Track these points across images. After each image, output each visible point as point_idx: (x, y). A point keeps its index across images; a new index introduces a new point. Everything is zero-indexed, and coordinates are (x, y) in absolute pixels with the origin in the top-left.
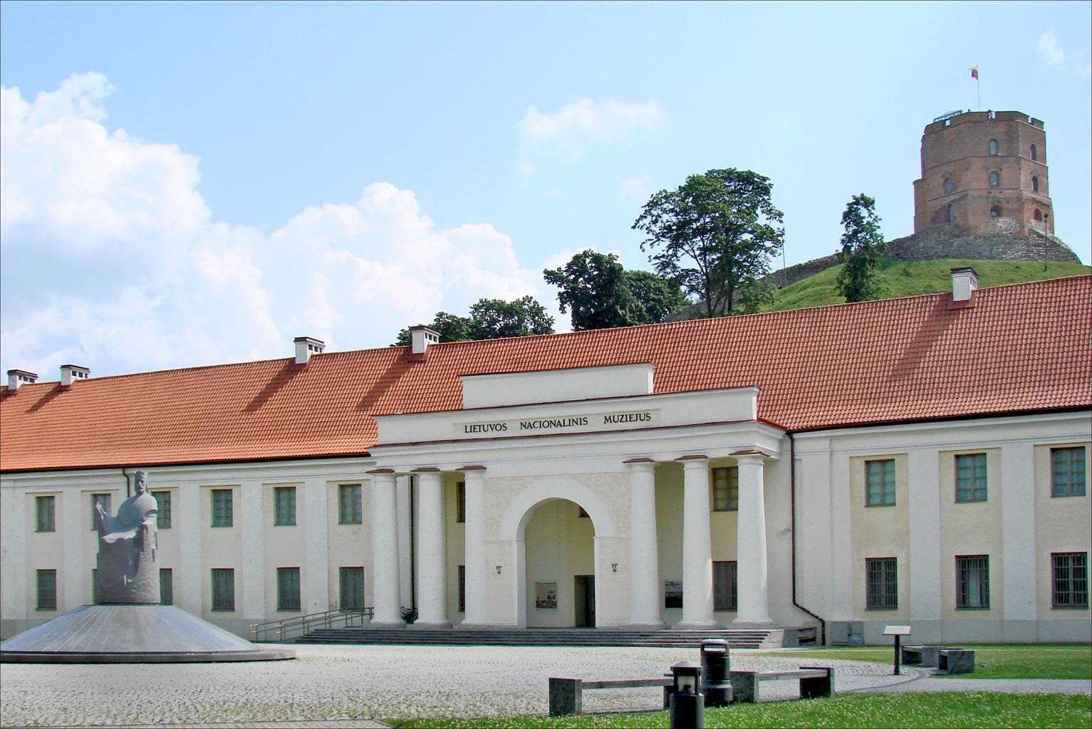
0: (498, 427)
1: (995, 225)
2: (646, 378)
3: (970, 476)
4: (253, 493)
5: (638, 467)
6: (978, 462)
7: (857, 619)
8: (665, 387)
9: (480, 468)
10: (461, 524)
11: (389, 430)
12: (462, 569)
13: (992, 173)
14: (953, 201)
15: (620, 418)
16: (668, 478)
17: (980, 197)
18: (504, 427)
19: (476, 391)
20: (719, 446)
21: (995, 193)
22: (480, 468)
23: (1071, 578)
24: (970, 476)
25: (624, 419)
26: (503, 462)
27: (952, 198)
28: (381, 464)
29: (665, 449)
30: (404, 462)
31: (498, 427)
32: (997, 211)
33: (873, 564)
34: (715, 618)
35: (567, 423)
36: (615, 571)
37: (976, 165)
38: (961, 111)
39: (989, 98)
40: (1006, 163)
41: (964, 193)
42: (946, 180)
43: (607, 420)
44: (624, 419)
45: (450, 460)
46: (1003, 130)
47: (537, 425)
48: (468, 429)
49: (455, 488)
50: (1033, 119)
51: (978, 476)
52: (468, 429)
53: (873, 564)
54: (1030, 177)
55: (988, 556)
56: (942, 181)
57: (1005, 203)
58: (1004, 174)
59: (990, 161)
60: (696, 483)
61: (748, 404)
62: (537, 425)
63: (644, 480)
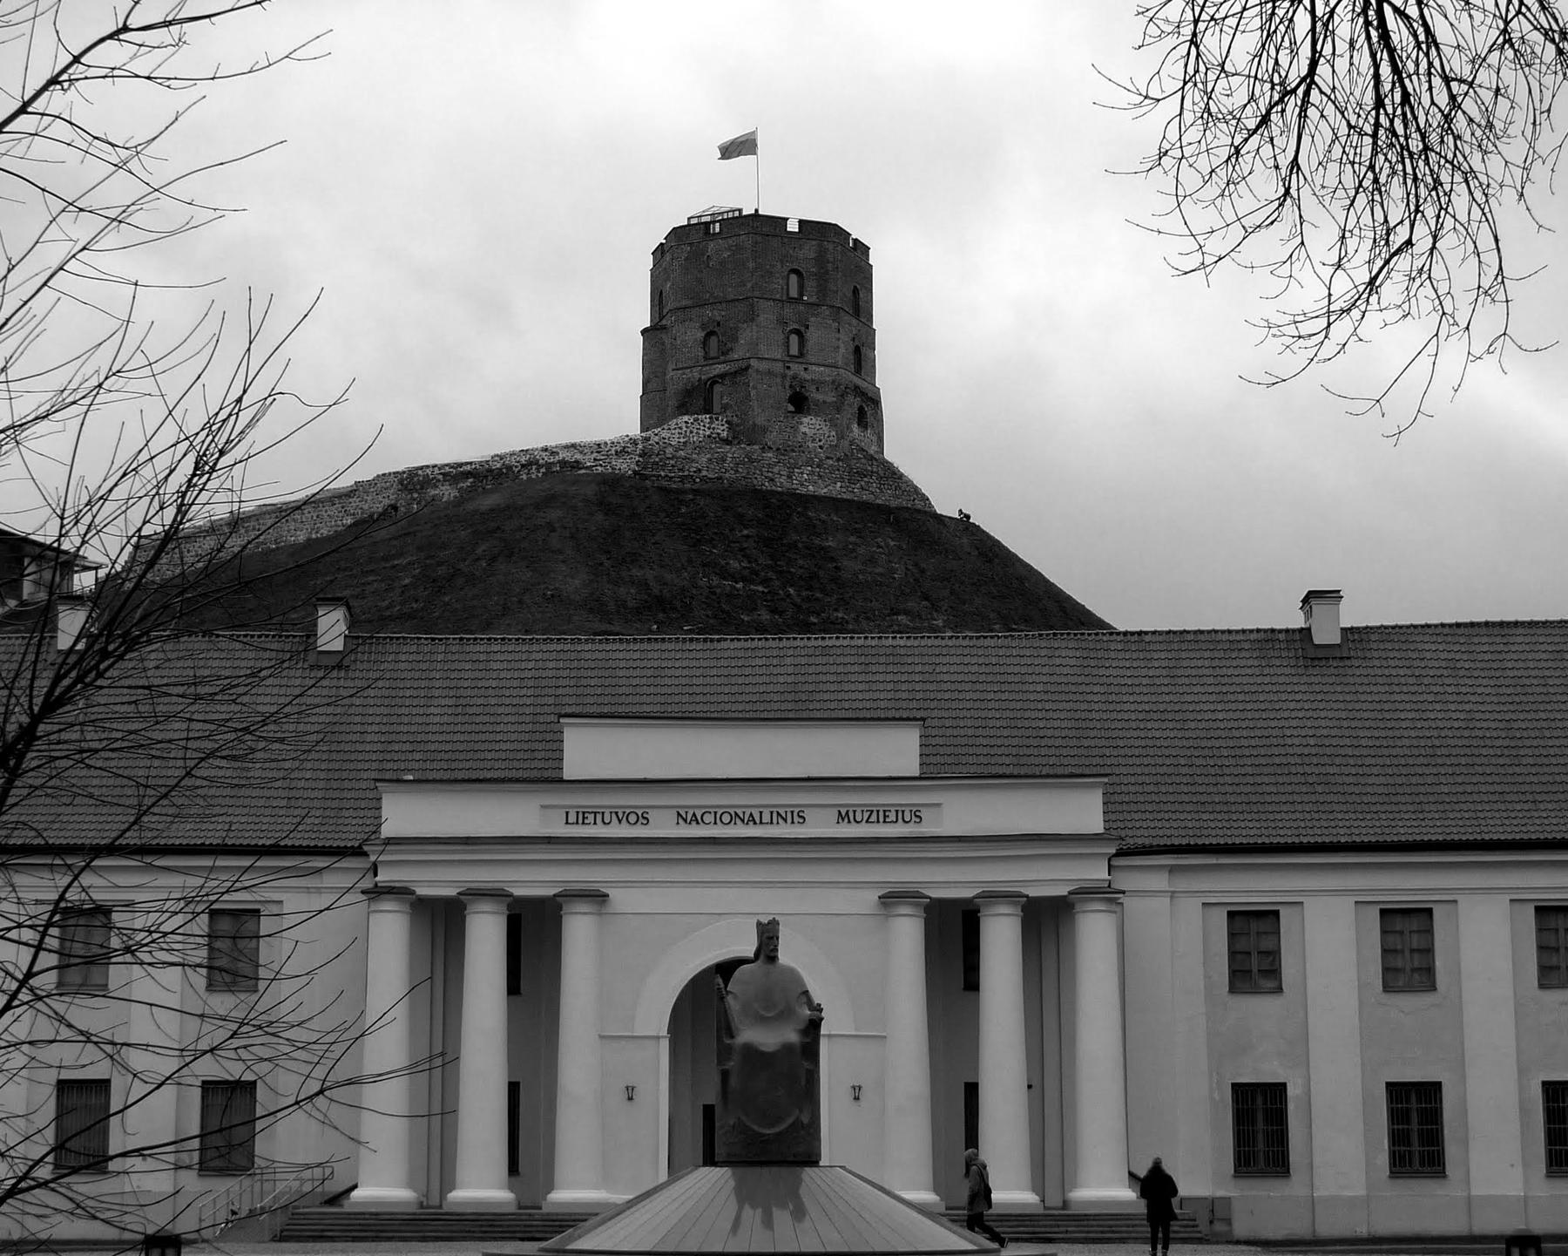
0: (633, 818)
1: (795, 429)
2: (897, 750)
3: (1408, 950)
4: (1330, 929)
5: (388, 905)
6: (1263, 925)
7: (1220, 1193)
8: (943, 767)
9: (597, 897)
10: (971, 994)
11: (404, 814)
12: (972, 1091)
13: (792, 332)
14: (722, 376)
15: (866, 815)
16: (954, 936)
17: (770, 373)
18: (644, 819)
19: (589, 750)
20: (1048, 878)
21: (796, 368)
22: (597, 897)
23: (1415, 1126)
24: (1408, 950)
25: (874, 817)
26: (639, 896)
27: (720, 369)
28: (384, 876)
29: (953, 881)
30: (437, 882)
31: (633, 818)
32: (800, 403)
33: (1243, 1093)
34: (511, 1188)
35: (766, 818)
36: (630, 1099)
37: (767, 314)
38: (740, 210)
39: (785, 192)
40: (816, 316)
41: (743, 364)
42: (710, 334)
43: (842, 817)
44: (874, 817)
45: (533, 880)
46: (813, 255)
47: (709, 818)
48: (572, 819)
49: (533, 933)
50: (856, 240)
51: (1415, 946)
52: (572, 819)
53: (1243, 1093)
54: (851, 348)
55: (1284, 1085)
56: (701, 335)
57: (813, 388)
58: (813, 336)
59: (788, 311)
60: (486, 937)
61: (1082, 811)
62: (709, 818)
63: (907, 935)
